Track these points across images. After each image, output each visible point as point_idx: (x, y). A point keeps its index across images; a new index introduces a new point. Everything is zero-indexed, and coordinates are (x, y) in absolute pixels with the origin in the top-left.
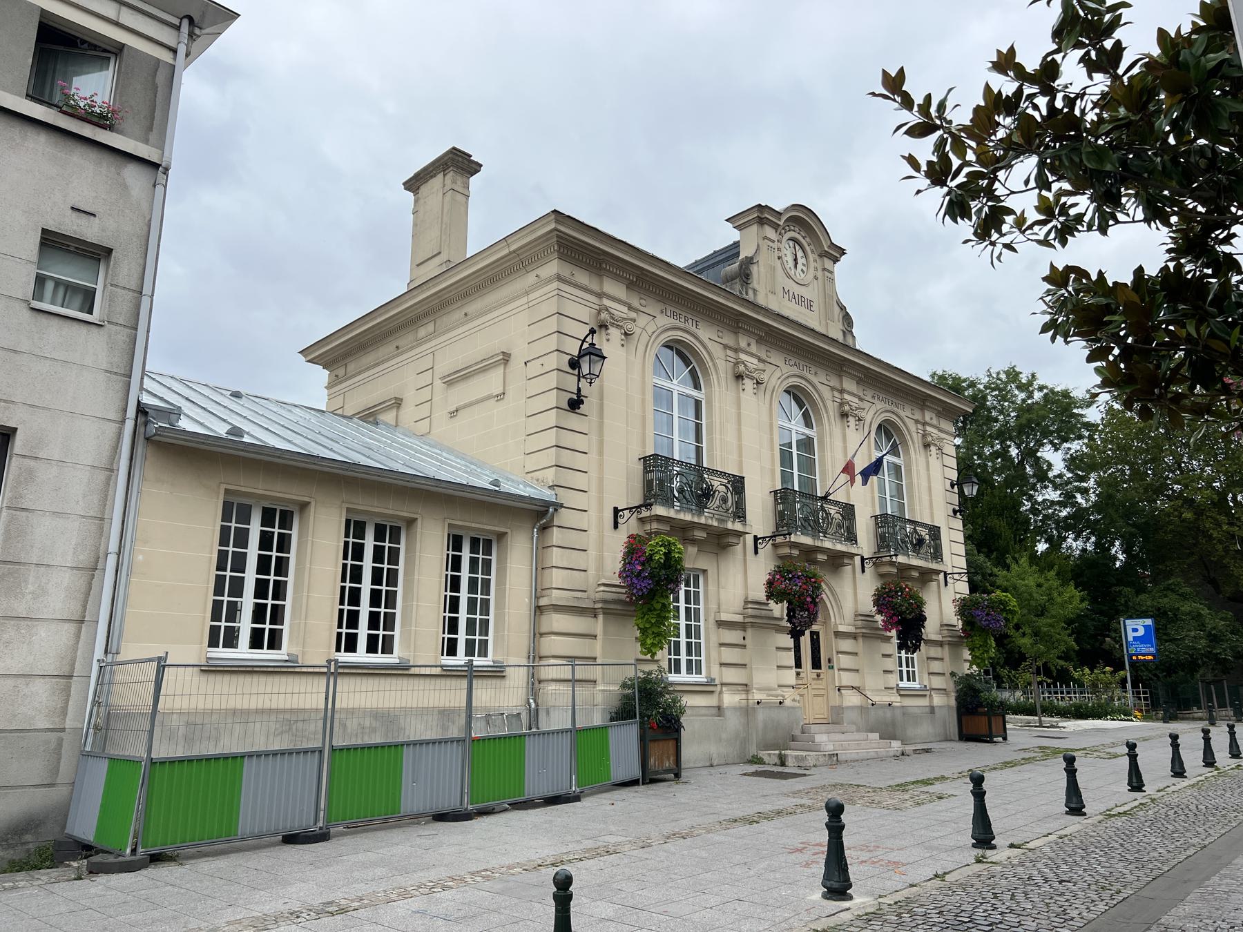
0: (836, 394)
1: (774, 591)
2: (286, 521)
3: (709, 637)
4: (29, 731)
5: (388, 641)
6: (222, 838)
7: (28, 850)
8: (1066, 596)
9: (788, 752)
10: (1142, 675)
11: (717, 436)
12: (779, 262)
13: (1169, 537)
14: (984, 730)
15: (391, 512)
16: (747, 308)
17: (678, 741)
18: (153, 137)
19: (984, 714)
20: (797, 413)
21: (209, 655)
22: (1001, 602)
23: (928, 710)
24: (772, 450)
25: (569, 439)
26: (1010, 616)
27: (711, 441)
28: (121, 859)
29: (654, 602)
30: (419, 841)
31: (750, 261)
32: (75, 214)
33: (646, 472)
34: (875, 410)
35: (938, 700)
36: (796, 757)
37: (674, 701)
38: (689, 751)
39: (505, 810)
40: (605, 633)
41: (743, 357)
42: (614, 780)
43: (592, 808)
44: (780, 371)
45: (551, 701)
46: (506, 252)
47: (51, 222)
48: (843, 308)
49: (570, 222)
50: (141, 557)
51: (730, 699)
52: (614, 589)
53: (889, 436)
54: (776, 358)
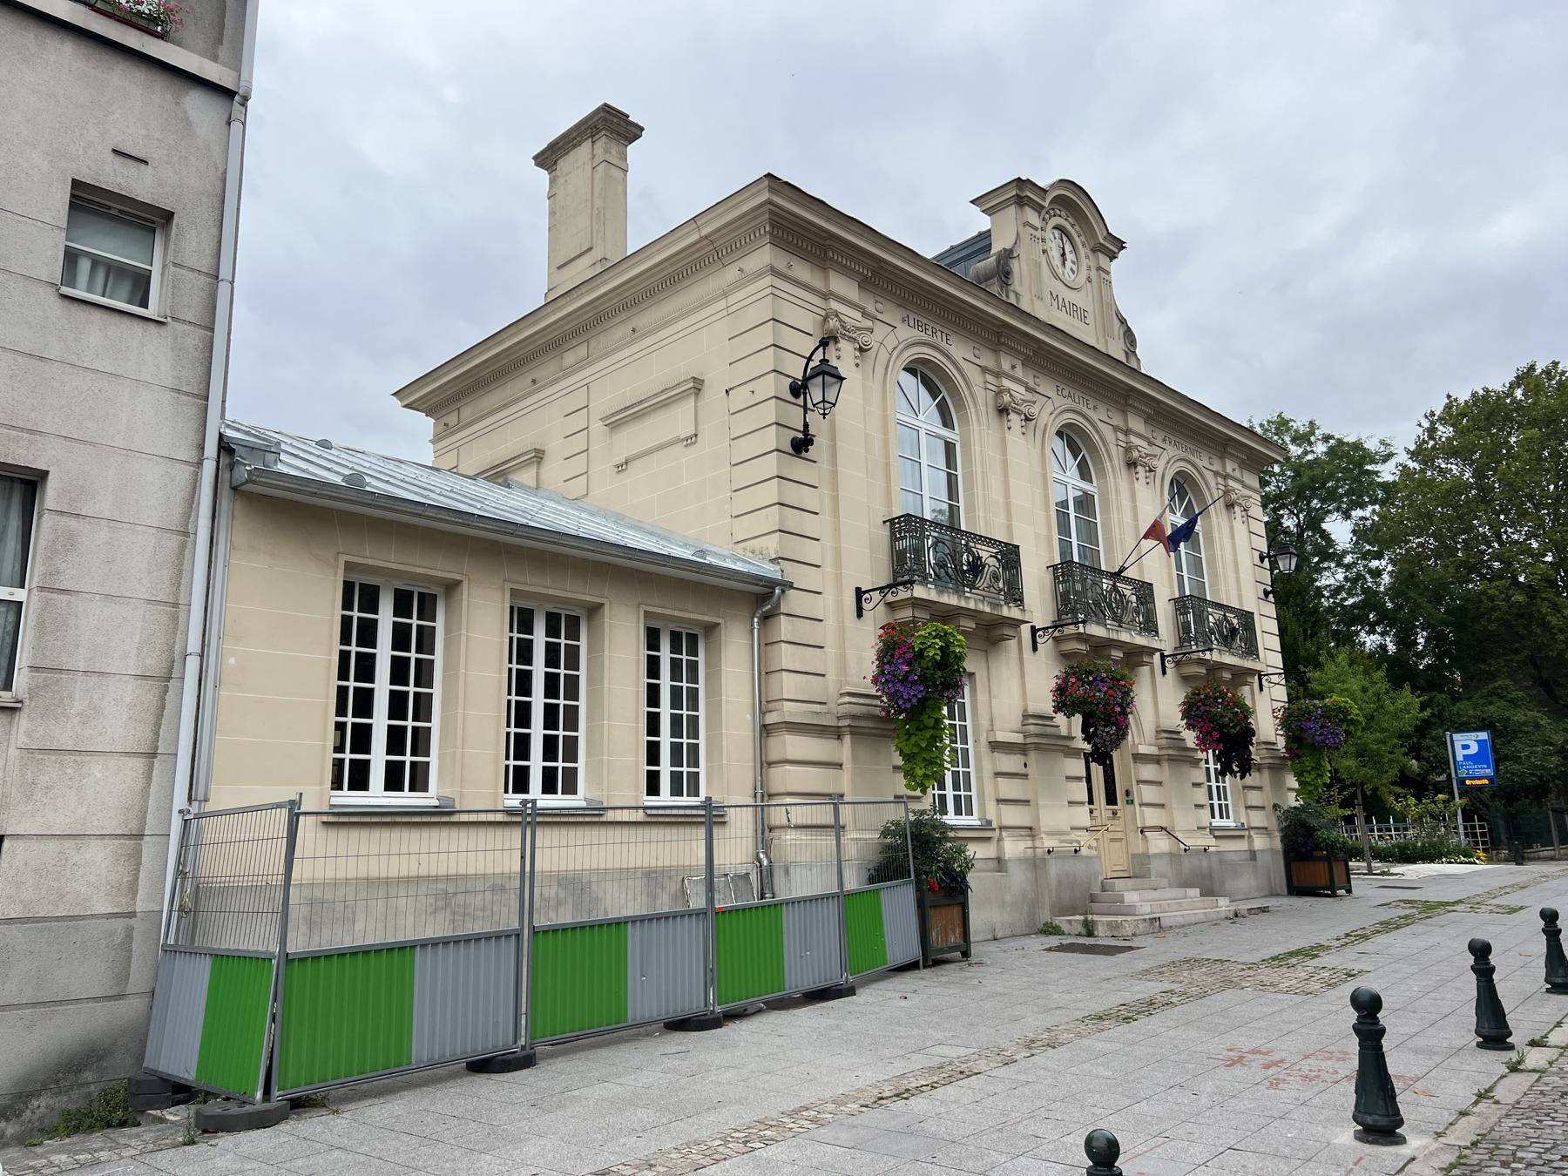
0: (1121, 436)
1: (1065, 702)
2: (427, 611)
3: (981, 764)
4: (83, 917)
5: (571, 775)
6: (390, 1073)
7: (89, 1094)
8: (1400, 703)
9: (1096, 918)
10: (1477, 805)
11: (979, 491)
12: (1043, 258)
13: (1494, 626)
14: (1323, 880)
15: (570, 595)
16: (1012, 315)
17: (964, 907)
18: (223, 52)
19: (1321, 859)
20: (1072, 463)
21: (334, 801)
22: (1340, 710)
23: (1247, 855)
24: (1047, 509)
25: (795, 495)
26: (1352, 728)
27: (970, 498)
28: (248, 1108)
29: (924, 718)
30: (669, 1063)
31: (1007, 255)
32: (119, 160)
33: (894, 538)
34: (1168, 458)
35: (1259, 842)
36: (1109, 924)
37: (960, 851)
38: (980, 916)
39: (760, 1011)
40: (855, 759)
41: (1006, 383)
42: (891, 963)
43: (878, 1004)
44: (1053, 404)
45: (791, 855)
46: (695, 237)
47: (85, 171)
48: (1123, 321)
49: (788, 191)
50: (232, 660)
51: (1013, 848)
52: (862, 701)
53: (1182, 494)
54: (1047, 387)
